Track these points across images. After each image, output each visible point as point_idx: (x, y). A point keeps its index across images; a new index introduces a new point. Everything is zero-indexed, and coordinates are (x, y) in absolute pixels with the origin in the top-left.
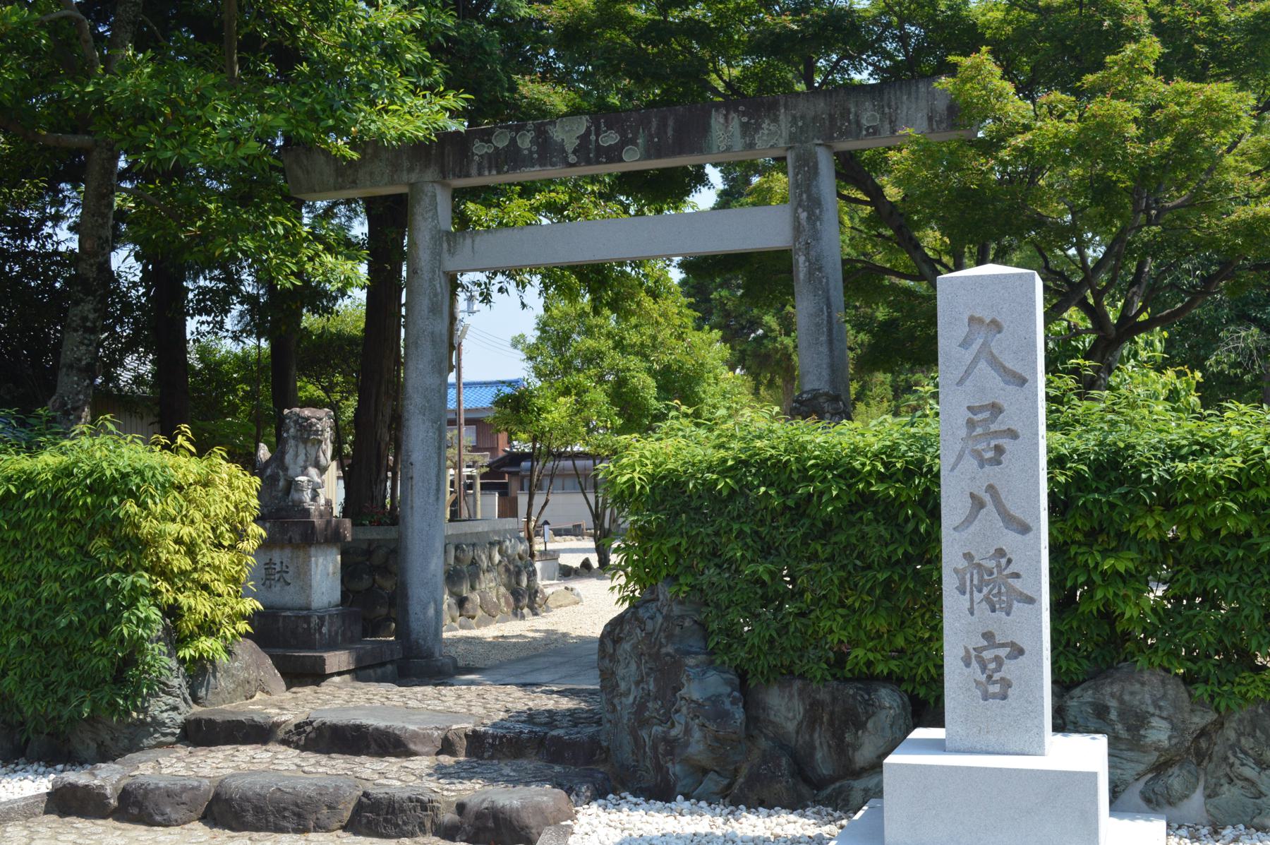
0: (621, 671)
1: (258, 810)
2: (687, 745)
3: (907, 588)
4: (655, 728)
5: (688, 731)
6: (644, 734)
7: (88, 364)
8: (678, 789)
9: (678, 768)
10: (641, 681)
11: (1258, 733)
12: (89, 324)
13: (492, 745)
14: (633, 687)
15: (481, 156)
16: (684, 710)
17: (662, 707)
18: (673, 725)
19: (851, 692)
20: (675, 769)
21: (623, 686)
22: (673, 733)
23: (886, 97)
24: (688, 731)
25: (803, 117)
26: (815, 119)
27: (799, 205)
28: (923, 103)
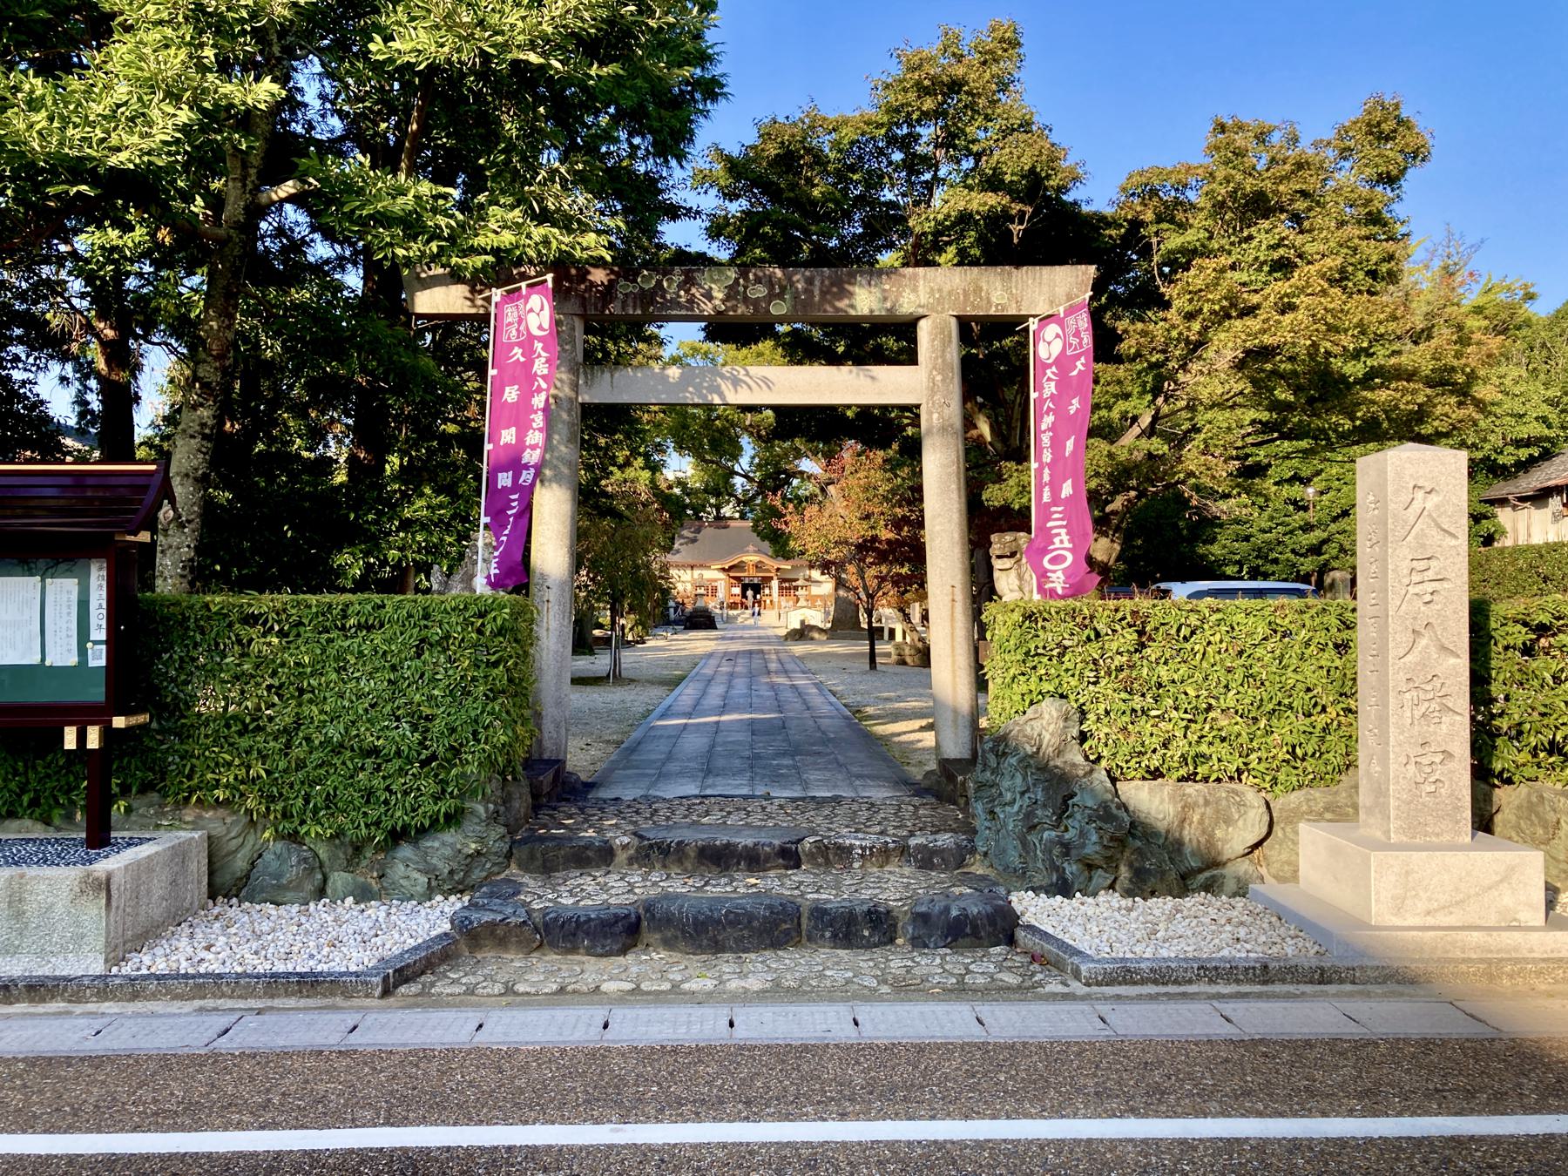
0: (1006, 784)
1: (975, 934)
2: (1083, 846)
3: (493, 708)
4: (1046, 835)
5: (1083, 834)
6: (1032, 838)
7: (204, 474)
8: (1076, 887)
9: (1074, 867)
10: (1028, 790)
11: (1533, 817)
12: (207, 431)
13: (862, 856)
14: (1018, 796)
15: (626, 295)
16: (1078, 816)
17: (1054, 813)
18: (1066, 830)
19: (1224, 795)
20: (1071, 869)
21: (1008, 796)
22: (1067, 836)
23: (1014, 279)
24: (1083, 834)
25: (940, 290)
26: (950, 293)
27: (934, 368)
28: (1045, 289)
